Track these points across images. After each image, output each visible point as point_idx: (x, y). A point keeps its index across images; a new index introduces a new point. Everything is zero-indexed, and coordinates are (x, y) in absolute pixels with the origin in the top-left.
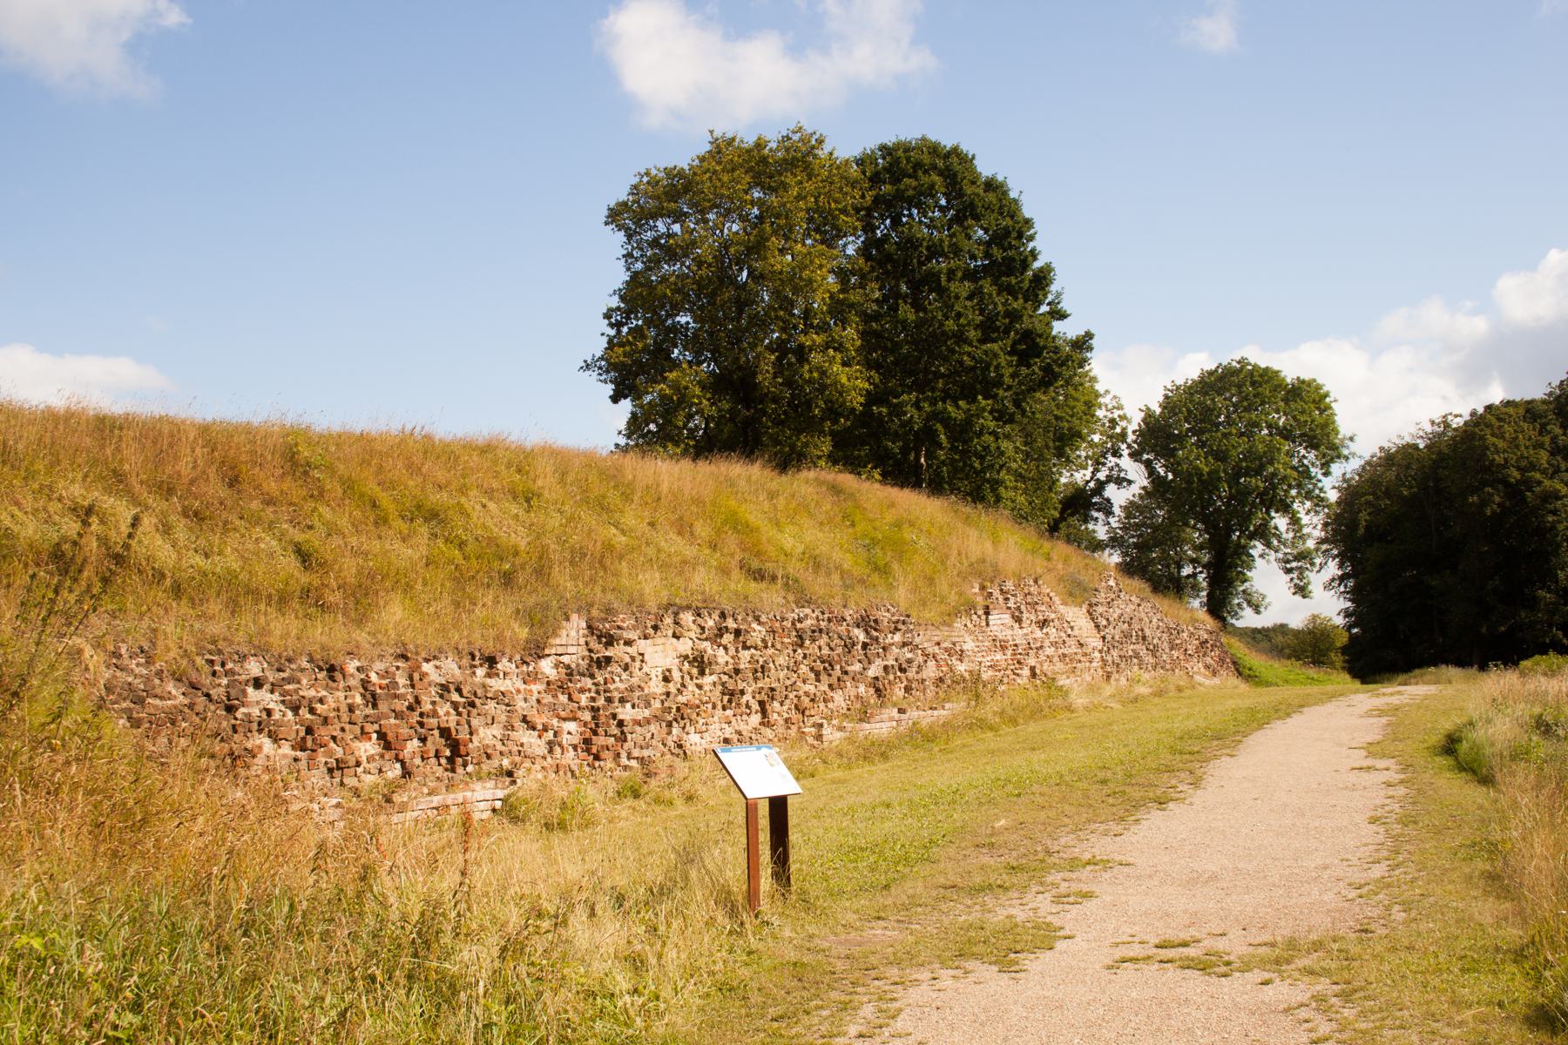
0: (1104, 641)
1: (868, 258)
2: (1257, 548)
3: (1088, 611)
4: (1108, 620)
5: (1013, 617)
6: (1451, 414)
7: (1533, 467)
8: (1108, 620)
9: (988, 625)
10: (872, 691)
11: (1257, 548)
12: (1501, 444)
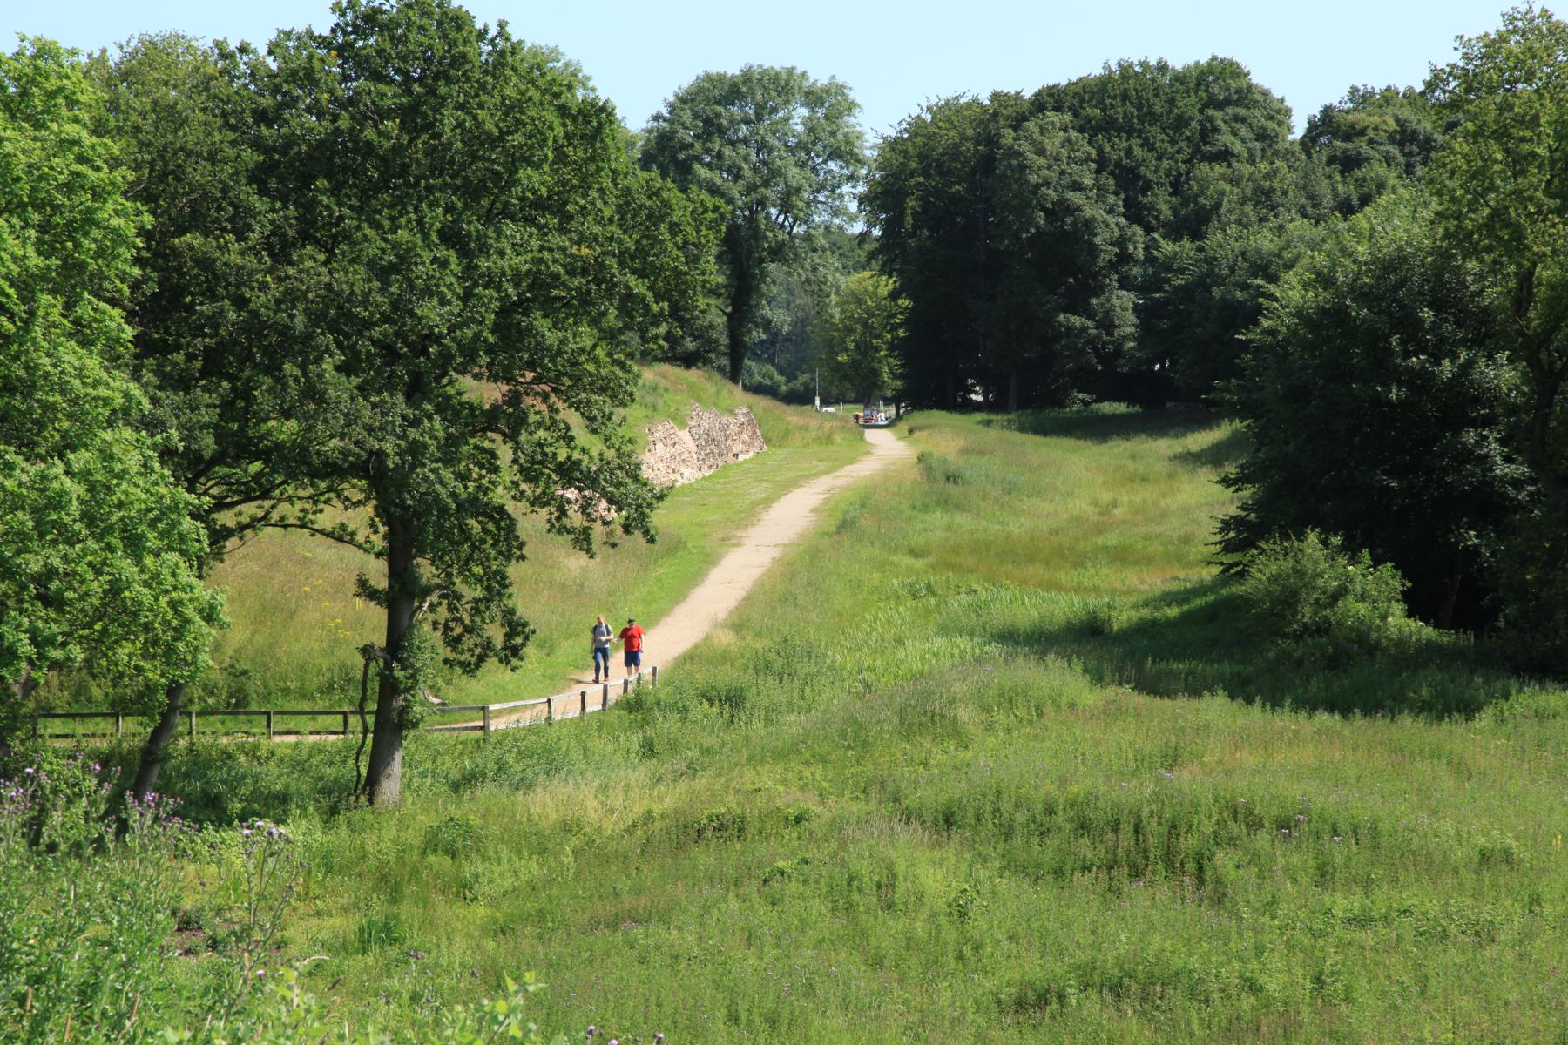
7: (1077, 186)
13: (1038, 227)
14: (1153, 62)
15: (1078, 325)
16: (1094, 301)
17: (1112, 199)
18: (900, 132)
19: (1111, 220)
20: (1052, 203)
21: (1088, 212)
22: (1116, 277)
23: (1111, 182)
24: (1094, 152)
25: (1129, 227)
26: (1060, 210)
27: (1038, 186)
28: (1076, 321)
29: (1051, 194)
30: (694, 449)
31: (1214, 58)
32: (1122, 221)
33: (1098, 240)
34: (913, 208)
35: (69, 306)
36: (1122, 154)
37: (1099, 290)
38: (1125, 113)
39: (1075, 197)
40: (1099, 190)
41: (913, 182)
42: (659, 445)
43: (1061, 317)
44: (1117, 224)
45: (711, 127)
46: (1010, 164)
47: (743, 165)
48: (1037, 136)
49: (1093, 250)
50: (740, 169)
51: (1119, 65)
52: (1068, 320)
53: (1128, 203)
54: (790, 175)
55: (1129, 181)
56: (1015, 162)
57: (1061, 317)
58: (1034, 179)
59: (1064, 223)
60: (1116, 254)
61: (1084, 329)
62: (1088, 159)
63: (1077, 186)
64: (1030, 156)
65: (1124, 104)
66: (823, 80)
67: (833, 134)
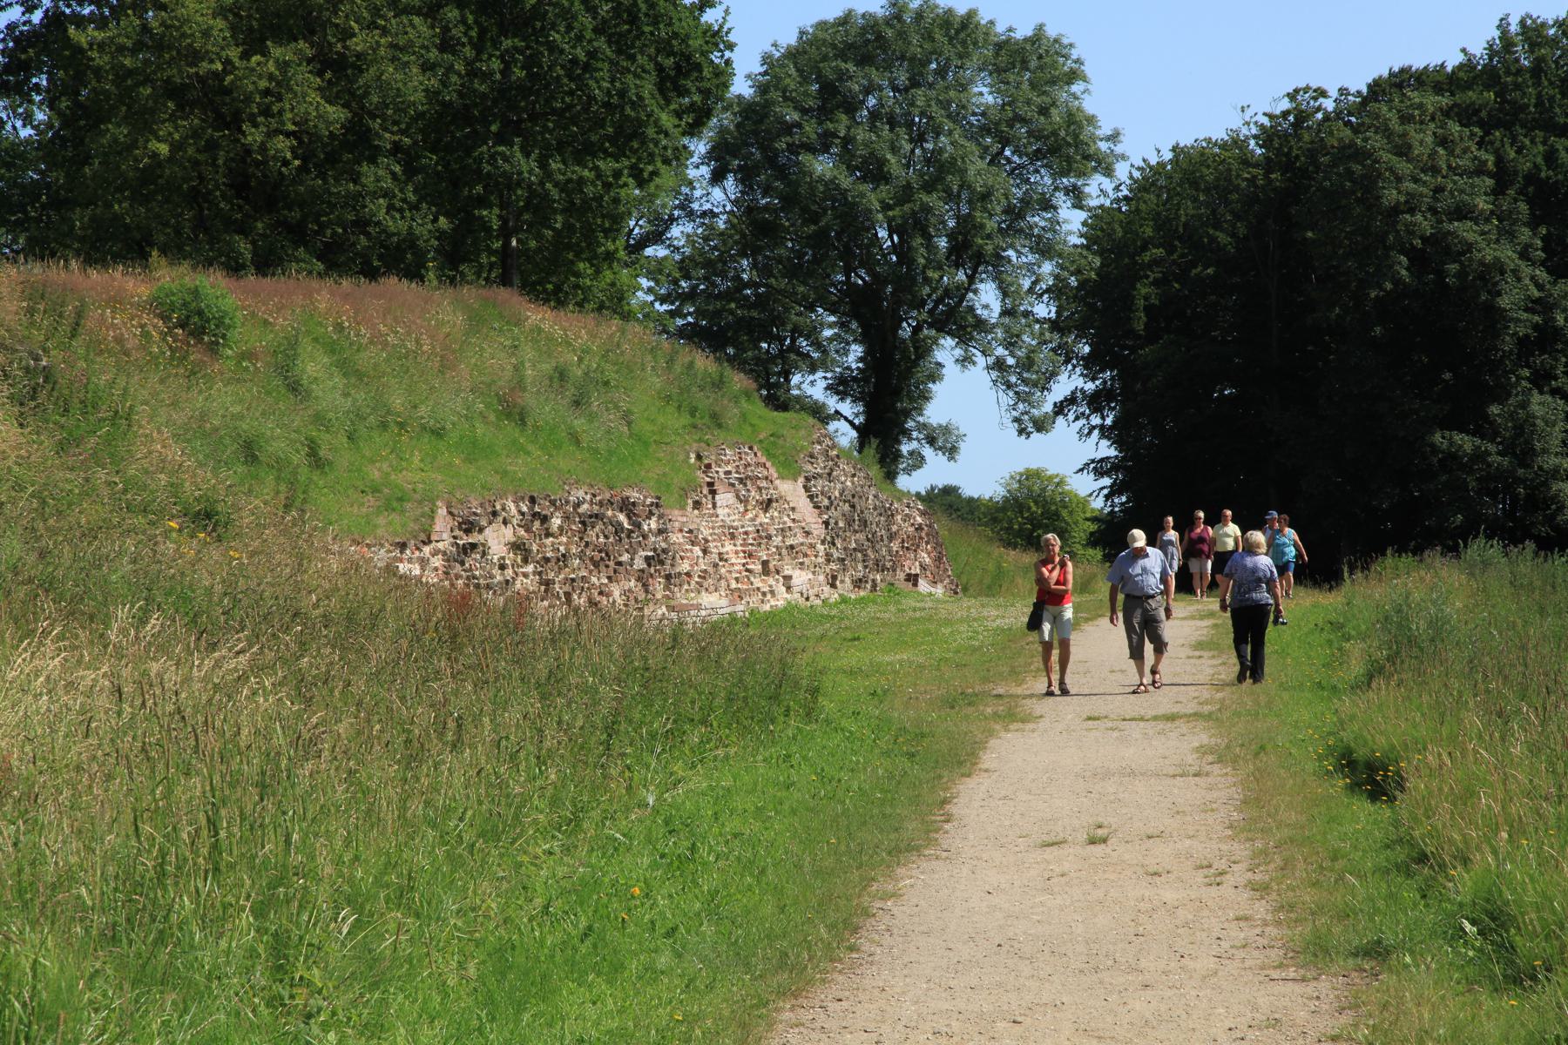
0: (827, 528)
1: (738, 131)
2: (946, 351)
3: (805, 487)
4: (830, 498)
5: (738, 497)
6: (1306, 89)
7: (1462, 212)
8: (830, 498)
9: (714, 506)
10: (640, 585)
11: (946, 351)
12: (1404, 167)
13: (1397, 281)
15: (1468, 447)
16: (1494, 409)
17: (1525, 234)
18: (1118, 200)
19: (1526, 270)
20: (1424, 239)
21: (1489, 254)
22: (1526, 373)
23: (1523, 207)
24: (1490, 159)
25: (1555, 283)
26: (1437, 250)
27: (1395, 211)
28: (1466, 443)
29: (1424, 223)
30: (818, 530)
32: (1542, 274)
33: (1504, 302)
34: (1146, 298)
36: (1539, 160)
37: (1501, 393)
38: (1539, 96)
39: (1466, 231)
40: (1500, 220)
41: (1147, 256)
42: (725, 498)
43: (1437, 437)
44: (1532, 278)
45: (834, 99)
46: (1349, 172)
47: (889, 156)
48: (1395, 124)
49: (1494, 318)
50: (882, 162)
51: (1522, 23)
52: (1452, 443)
54: (971, 172)
56: (1357, 168)
57: (1437, 437)
58: (1391, 196)
59: (1441, 274)
60: (1536, 327)
61: (1479, 456)
62: (1480, 171)
63: (1462, 212)
64: (1385, 156)
65: (1538, 84)
66: (1023, 31)
67: (1044, 111)
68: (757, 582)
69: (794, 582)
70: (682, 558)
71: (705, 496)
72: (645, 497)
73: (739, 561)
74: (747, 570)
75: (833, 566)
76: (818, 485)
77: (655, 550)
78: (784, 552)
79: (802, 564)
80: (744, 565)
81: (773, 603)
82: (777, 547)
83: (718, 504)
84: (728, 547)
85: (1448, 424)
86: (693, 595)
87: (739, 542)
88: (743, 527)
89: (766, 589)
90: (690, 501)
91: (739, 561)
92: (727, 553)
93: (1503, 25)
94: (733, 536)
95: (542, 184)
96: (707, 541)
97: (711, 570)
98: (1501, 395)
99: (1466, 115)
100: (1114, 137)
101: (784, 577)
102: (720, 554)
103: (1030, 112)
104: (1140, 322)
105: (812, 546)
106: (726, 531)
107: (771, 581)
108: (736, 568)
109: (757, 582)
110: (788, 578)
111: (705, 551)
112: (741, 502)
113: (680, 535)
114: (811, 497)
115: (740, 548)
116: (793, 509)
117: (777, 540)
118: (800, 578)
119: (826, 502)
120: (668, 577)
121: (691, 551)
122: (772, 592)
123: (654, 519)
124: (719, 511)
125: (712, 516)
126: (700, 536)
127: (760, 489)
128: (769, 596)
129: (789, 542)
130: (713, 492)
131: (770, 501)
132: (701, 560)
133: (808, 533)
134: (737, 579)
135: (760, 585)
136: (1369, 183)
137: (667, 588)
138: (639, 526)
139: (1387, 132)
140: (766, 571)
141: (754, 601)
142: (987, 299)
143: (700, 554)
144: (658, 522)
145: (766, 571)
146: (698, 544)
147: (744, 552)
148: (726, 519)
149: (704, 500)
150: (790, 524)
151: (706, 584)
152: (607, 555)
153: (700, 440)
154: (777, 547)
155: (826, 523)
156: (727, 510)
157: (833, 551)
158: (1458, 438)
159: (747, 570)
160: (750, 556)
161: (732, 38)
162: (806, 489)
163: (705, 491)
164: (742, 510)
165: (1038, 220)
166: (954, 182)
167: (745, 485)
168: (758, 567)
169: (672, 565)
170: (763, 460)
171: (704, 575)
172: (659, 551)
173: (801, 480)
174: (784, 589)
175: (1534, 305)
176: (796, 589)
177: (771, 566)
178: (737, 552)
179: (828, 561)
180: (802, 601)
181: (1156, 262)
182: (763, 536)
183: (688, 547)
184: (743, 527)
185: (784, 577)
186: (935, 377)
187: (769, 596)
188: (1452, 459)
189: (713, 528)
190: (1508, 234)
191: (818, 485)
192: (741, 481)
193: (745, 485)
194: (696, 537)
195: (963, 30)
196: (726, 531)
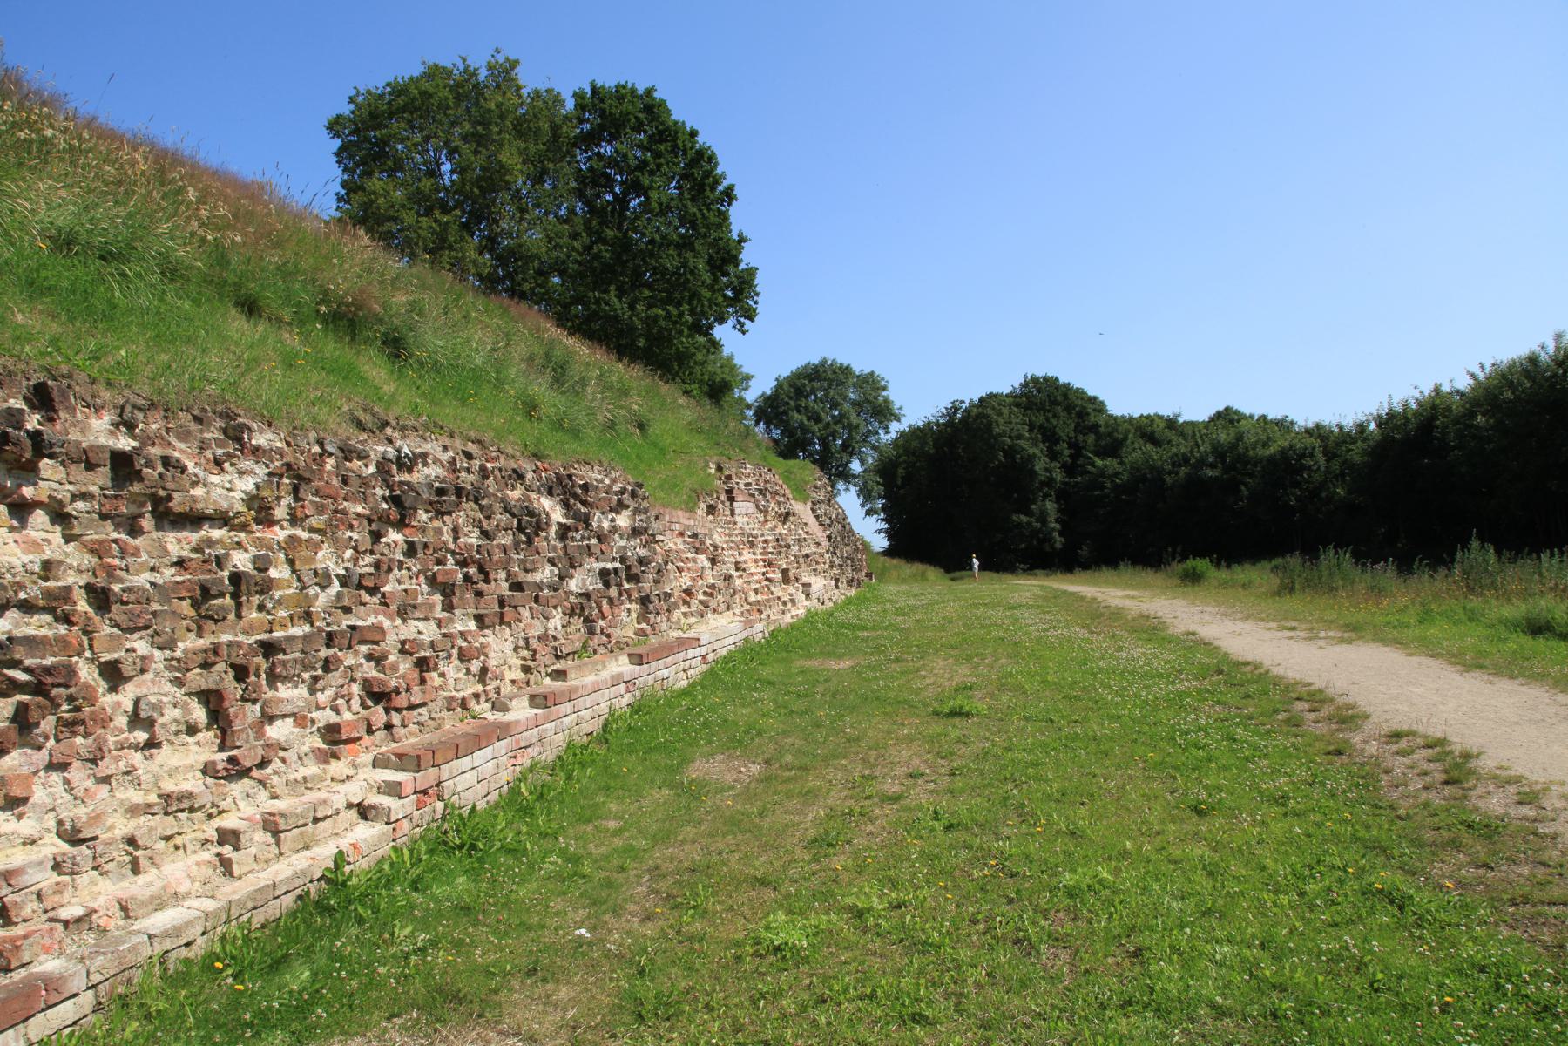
5: (757, 507)
7: (1020, 437)
9: (733, 513)
14: (1290, 419)
16: (1033, 507)
17: (1041, 445)
21: (1031, 451)
26: (1010, 452)
28: (1024, 518)
30: (825, 543)
31: (824, 361)
33: (1037, 468)
35: (399, 451)
39: (1022, 443)
42: (743, 507)
49: (1033, 473)
53: (1050, 449)
55: (1050, 437)
58: (997, 430)
61: (1029, 523)
62: (1024, 424)
63: (1020, 437)
68: (778, 591)
69: (814, 588)
70: (680, 570)
71: (723, 503)
72: (614, 481)
73: (759, 570)
74: (767, 579)
75: (836, 571)
76: (821, 509)
77: (623, 560)
78: (801, 560)
79: (815, 570)
80: (764, 574)
81: (794, 613)
82: (795, 556)
83: (737, 512)
84: (747, 556)
85: (1019, 512)
86: (692, 620)
87: (760, 550)
88: (762, 535)
89: (787, 598)
90: (703, 506)
91: (759, 570)
92: (745, 562)
93: (1025, 377)
94: (752, 545)
95: (630, 318)
96: (716, 547)
97: (720, 584)
98: (1034, 501)
99: (1018, 405)
100: (900, 408)
101: (804, 585)
102: (737, 563)
103: (871, 398)
104: (899, 482)
105: (821, 555)
106: (745, 539)
107: (791, 589)
108: (755, 578)
109: (778, 591)
110: (807, 586)
111: (713, 561)
112: (761, 512)
113: (679, 540)
114: (817, 517)
115: (759, 557)
116: (806, 524)
117: (795, 549)
118: (818, 584)
119: (828, 521)
120: (645, 601)
121: (694, 560)
122: (793, 601)
123: (626, 513)
124: (738, 519)
125: (729, 522)
126: (708, 542)
127: (779, 503)
128: (789, 605)
129: (805, 551)
130: (731, 499)
131: (788, 514)
132: (708, 572)
133: (818, 544)
134: (756, 591)
135: (780, 594)
136: (989, 425)
137: (642, 617)
138: (586, 521)
139: (994, 408)
140: (786, 578)
141: (773, 612)
142: (856, 466)
143: (707, 564)
144: (633, 518)
145: (786, 578)
146: (704, 552)
147: (764, 561)
148: (745, 527)
149: (720, 506)
150: (804, 536)
151: (713, 603)
152: (482, 570)
153: (721, 454)
154: (795, 556)
155: (829, 537)
156: (746, 519)
157: (835, 558)
158: (1022, 517)
159: (767, 579)
160: (770, 565)
161: (758, 289)
162: (813, 511)
163: (723, 497)
164: (762, 519)
165: (872, 439)
166: (846, 421)
167: (765, 496)
168: (778, 576)
169: (656, 582)
170: (781, 482)
171: (711, 591)
172: (632, 561)
173: (809, 504)
174: (803, 596)
175: (1047, 470)
176: (814, 596)
177: (791, 574)
178: (756, 561)
179: (831, 567)
180: (820, 607)
181: (905, 462)
182: (781, 545)
183: (690, 555)
184: (762, 535)
185: (804, 585)
186: (910, 426)
187: (789, 605)
188: (1019, 524)
189: (730, 535)
190: (1036, 446)
191: (821, 509)
192: (761, 492)
193: (765, 496)
194: (702, 543)
195: (846, 370)
196: (745, 539)
